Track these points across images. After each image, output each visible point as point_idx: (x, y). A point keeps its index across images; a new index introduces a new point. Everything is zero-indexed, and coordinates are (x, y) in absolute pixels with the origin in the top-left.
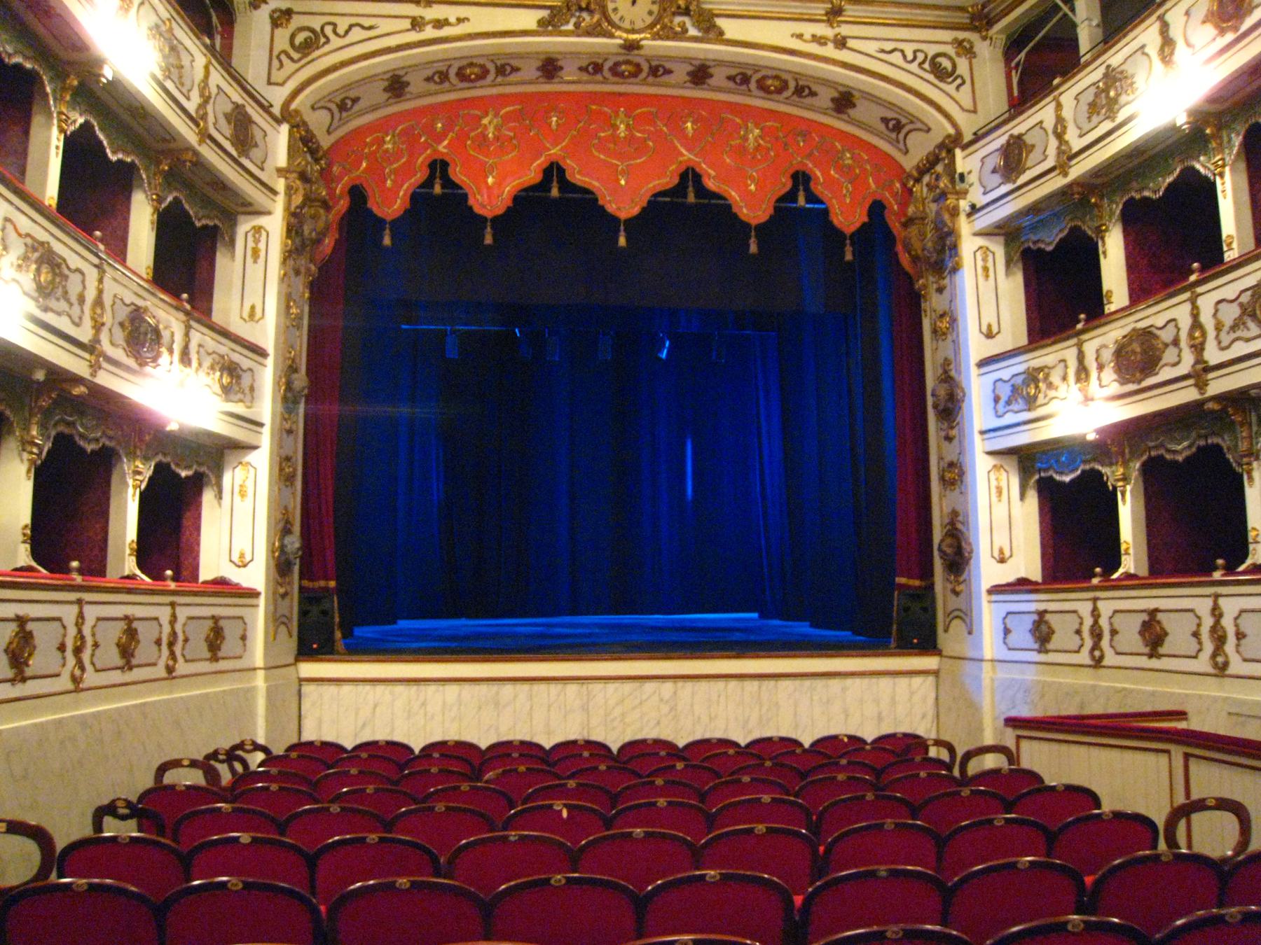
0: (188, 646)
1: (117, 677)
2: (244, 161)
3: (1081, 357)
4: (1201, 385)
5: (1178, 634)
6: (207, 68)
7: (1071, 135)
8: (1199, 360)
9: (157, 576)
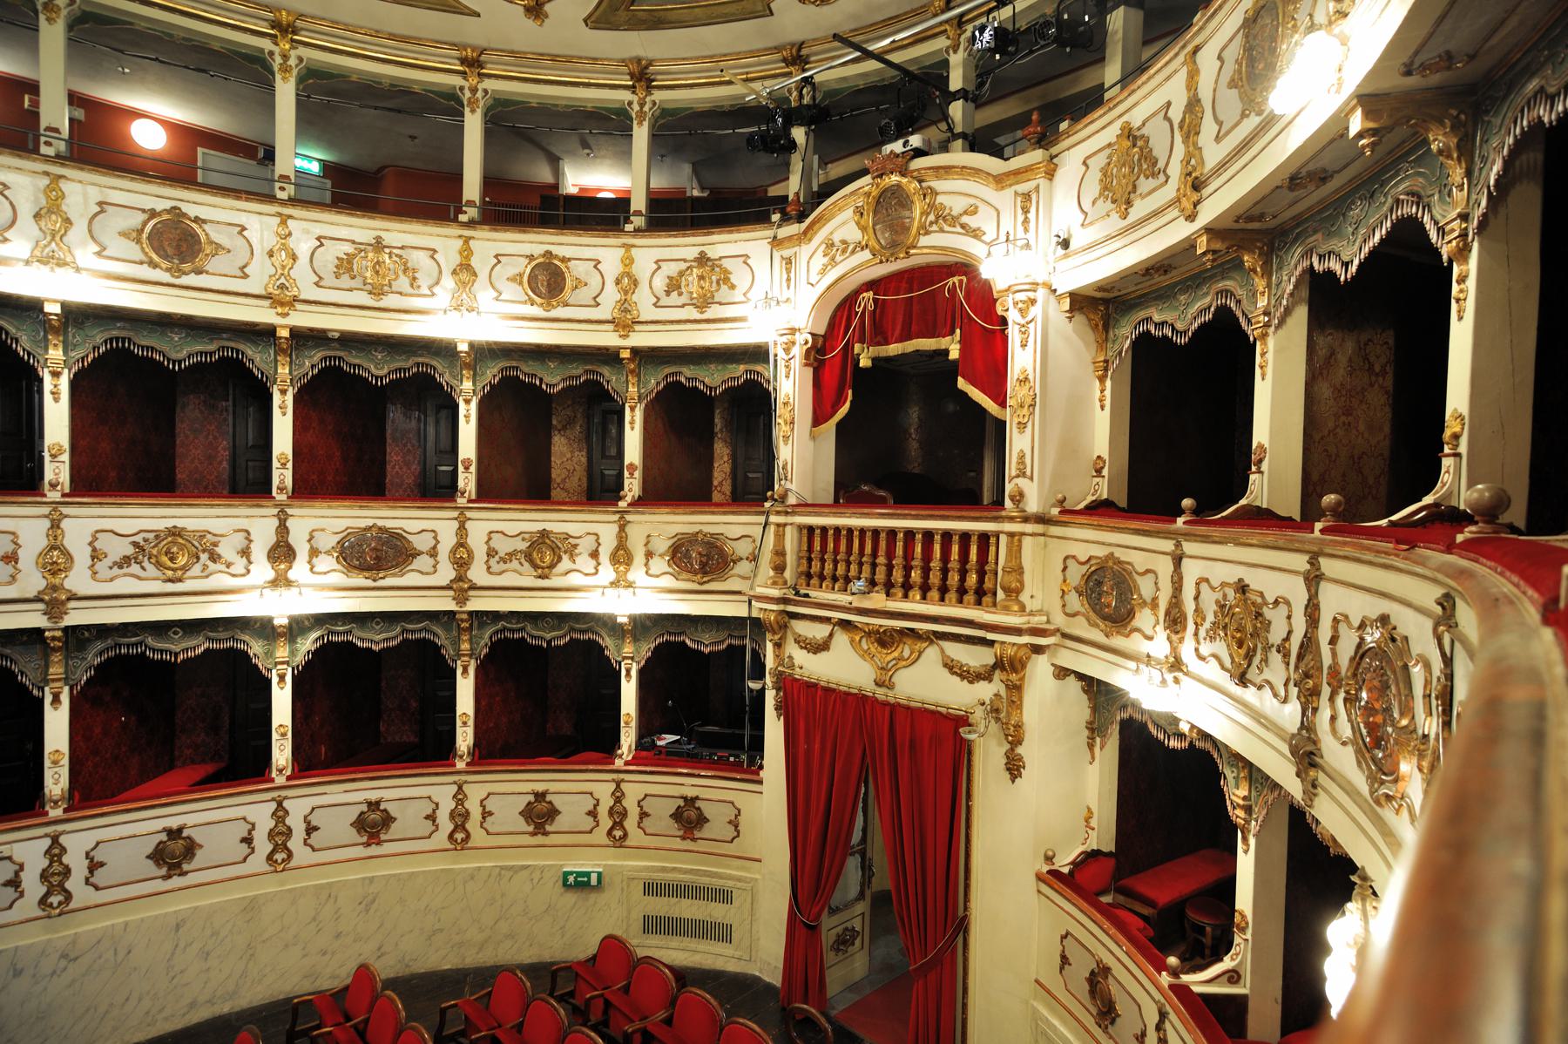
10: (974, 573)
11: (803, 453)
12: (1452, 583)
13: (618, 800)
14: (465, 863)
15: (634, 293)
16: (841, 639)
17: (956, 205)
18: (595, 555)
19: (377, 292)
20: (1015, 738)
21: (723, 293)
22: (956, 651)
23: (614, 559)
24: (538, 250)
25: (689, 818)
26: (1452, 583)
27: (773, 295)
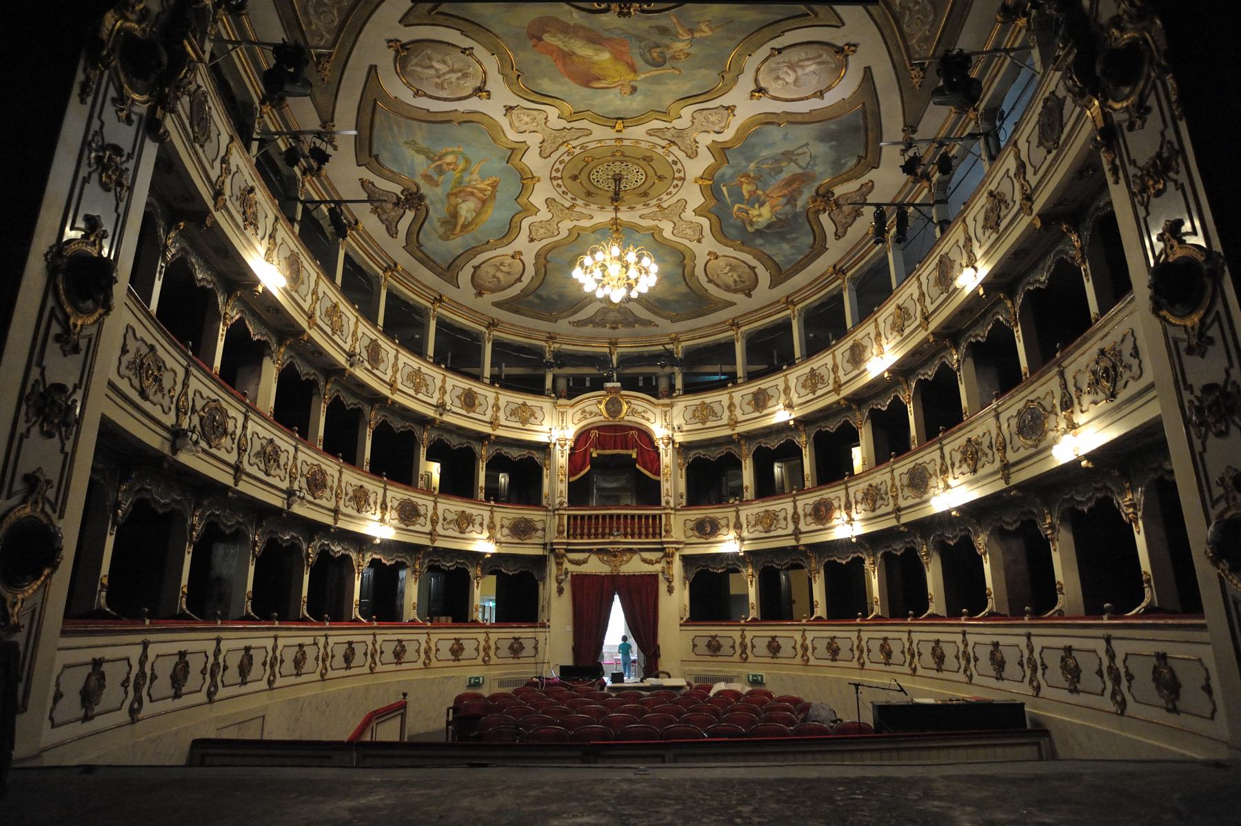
0: (156, 683)
1: (393, 667)
2: (375, 371)
4: (797, 540)
6: (356, 323)
8: (796, 528)
10: (653, 527)
11: (556, 484)
12: (403, 677)
13: (487, 642)
15: (495, 412)
16: (594, 559)
17: (640, 409)
18: (481, 525)
20: (669, 581)
21: (532, 419)
22: (646, 555)
24: (467, 387)
25: (516, 649)
26: (403, 677)
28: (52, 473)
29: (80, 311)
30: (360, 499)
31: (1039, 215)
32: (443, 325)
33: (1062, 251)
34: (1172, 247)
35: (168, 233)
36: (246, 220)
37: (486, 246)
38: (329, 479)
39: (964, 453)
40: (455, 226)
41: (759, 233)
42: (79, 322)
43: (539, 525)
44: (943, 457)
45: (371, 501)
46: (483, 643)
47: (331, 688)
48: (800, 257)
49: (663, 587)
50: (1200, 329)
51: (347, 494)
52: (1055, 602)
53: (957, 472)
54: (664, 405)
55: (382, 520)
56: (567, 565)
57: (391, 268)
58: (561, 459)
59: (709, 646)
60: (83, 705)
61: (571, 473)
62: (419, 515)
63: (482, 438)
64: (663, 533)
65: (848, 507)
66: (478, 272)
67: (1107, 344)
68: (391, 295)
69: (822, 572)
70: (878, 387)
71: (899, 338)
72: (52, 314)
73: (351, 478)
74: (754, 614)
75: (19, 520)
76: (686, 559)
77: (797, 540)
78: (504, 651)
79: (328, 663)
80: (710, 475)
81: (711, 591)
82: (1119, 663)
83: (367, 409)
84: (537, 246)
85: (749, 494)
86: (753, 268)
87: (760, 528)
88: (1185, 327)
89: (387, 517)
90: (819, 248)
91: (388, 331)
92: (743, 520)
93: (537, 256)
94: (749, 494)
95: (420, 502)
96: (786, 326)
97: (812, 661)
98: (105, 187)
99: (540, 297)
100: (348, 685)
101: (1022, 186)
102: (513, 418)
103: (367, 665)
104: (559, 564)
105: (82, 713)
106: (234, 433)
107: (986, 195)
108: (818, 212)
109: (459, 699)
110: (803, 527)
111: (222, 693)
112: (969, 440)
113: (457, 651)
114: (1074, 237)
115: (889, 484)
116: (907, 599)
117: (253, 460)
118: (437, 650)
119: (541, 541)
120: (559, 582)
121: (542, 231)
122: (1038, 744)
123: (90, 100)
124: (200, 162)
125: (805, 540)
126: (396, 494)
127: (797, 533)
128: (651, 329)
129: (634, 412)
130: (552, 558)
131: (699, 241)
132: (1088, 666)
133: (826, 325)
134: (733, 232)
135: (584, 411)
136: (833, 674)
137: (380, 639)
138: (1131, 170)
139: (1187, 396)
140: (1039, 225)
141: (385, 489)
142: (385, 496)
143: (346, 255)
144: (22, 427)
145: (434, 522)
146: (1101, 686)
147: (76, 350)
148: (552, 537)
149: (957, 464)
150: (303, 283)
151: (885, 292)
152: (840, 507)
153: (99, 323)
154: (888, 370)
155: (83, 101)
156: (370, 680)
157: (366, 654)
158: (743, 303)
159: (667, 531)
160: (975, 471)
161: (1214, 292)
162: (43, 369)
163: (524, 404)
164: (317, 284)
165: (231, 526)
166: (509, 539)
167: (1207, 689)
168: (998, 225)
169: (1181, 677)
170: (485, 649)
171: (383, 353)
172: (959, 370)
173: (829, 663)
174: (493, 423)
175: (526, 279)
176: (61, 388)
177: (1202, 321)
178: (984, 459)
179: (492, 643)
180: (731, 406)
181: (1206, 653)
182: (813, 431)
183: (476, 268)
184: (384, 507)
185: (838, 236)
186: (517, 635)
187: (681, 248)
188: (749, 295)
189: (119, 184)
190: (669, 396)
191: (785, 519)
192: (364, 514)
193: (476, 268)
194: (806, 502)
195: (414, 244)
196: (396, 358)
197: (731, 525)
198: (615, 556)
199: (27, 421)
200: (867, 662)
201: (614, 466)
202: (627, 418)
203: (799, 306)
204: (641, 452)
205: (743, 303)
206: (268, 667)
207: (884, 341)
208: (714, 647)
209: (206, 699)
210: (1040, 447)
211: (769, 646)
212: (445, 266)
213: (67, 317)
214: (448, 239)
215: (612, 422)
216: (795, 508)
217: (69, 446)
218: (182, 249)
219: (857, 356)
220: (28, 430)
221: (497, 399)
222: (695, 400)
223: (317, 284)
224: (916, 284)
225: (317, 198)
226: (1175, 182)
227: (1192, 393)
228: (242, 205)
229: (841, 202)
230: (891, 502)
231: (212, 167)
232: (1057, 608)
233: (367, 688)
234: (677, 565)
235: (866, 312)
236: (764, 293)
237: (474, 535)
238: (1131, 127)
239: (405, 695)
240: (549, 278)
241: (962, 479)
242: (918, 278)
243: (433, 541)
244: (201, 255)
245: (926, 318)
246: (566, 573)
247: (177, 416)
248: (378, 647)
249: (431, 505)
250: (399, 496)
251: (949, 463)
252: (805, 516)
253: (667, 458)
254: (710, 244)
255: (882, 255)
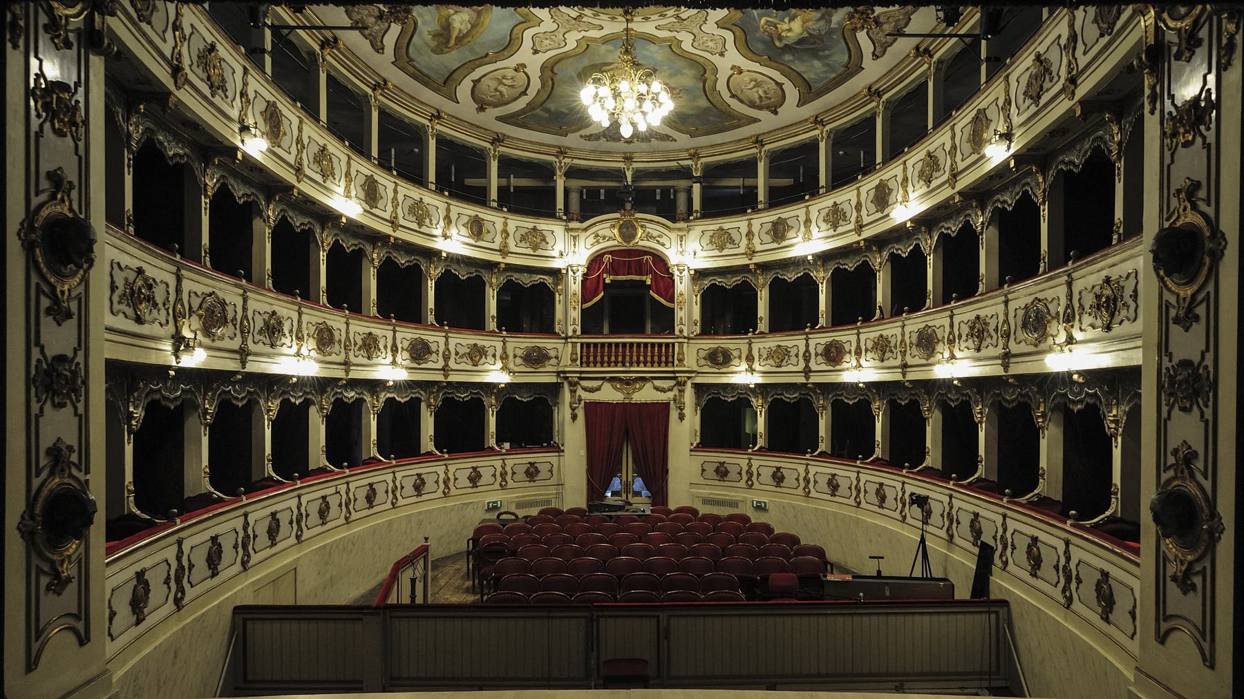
1: (415, 499)
3: (807, 213)
4: (807, 378)
5: (790, 479)
6: (349, 163)
7: (756, 240)
8: (807, 366)
9: (442, 325)
10: (666, 355)
11: (568, 311)
13: (503, 468)
14: (450, 503)
16: (607, 386)
17: (655, 234)
18: (494, 356)
19: (535, 249)
22: (657, 383)
23: (502, 358)
24: (473, 213)
25: (532, 473)
27: (571, 251)
28: (71, 439)
29: (62, 276)
30: (370, 345)
31: (1080, 102)
32: (442, 141)
33: (1101, 138)
34: (1185, 210)
35: (128, 119)
36: (211, 87)
37: (483, 60)
38: (336, 333)
39: (972, 328)
40: (448, 40)
41: (788, 48)
42: (66, 287)
43: (552, 353)
44: (952, 326)
45: (381, 346)
46: (499, 470)
47: (356, 529)
48: (833, 75)
49: (674, 414)
50: (1191, 303)
51: (355, 344)
52: (1036, 485)
53: (963, 345)
54: (680, 229)
55: (394, 363)
56: (580, 392)
57: (381, 85)
58: (575, 286)
59: (717, 471)
60: (134, 612)
61: (584, 300)
62: (430, 353)
63: (491, 266)
64: (676, 362)
65: (858, 353)
66: (479, 85)
67: (1114, 273)
68: (383, 114)
69: (829, 408)
70: (899, 234)
71: (924, 189)
72: (39, 290)
73: (359, 328)
74: (761, 442)
75: (51, 491)
76: (698, 388)
77: (807, 378)
78: (521, 475)
79: (351, 507)
80: (727, 306)
81: (723, 420)
82: (1073, 565)
83: (368, 248)
84: (542, 58)
85: (763, 326)
86: (780, 85)
87: (771, 362)
88: (1178, 295)
89: (399, 359)
90: (853, 68)
91: (384, 164)
92: (755, 353)
93: (543, 68)
94: (763, 326)
95: (431, 339)
96: (812, 146)
97: (813, 494)
98: (59, 133)
99: (548, 111)
100: (372, 523)
101: (1070, 63)
102: (523, 244)
103: (343, 515)
104: (573, 392)
105: (134, 619)
106: (234, 319)
107: (1032, 57)
108: (855, 30)
109: (479, 531)
110: (813, 366)
111: (255, 558)
112: (978, 317)
113: (475, 478)
114: (1115, 129)
115: (899, 338)
116: (905, 452)
117: (258, 337)
118: (456, 479)
119: (554, 369)
120: (573, 409)
121: (547, 42)
122: (997, 613)
123: (21, 43)
124: (151, 42)
125: (814, 379)
126: (407, 334)
127: (807, 371)
128: (669, 145)
129: (649, 237)
130: (566, 385)
131: (722, 54)
132: (1048, 558)
133: (853, 156)
134: (760, 46)
135: (597, 236)
136: (831, 508)
137: (399, 476)
138: (1168, 106)
139: (1165, 359)
140: (1078, 113)
141: (395, 332)
142: (394, 338)
143: (329, 76)
144: (35, 408)
145: (446, 358)
146: (1056, 579)
147: (69, 315)
148: (566, 363)
149: (964, 337)
150: (285, 134)
151: (918, 135)
152: (850, 352)
153: (85, 281)
154: (911, 220)
155: (15, 46)
156: (393, 515)
157: (387, 492)
158: (767, 121)
159: (679, 360)
160: (978, 350)
161: (1210, 270)
162: (42, 348)
163: (535, 229)
164: (300, 130)
165: (243, 399)
166: (523, 369)
167: (1133, 614)
168: (1039, 97)
169: (1117, 597)
170: (501, 475)
171: (381, 188)
172: (982, 233)
173: (828, 497)
174: (504, 251)
175: (532, 93)
176: (61, 359)
177: (1194, 296)
178: (989, 340)
179: (508, 469)
180: (750, 234)
181: (1136, 585)
182: (832, 266)
183: (476, 82)
184: (395, 350)
185: (875, 56)
186: (532, 460)
187: (701, 61)
188: (776, 113)
189: (73, 123)
190: (686, 220)
191: (797, 355)
192: (375, 361)
193: (476, 82)
194: (819, 341)
195: (403, 58)
196: (395, 191)
197: (744, 357)
198: (628, 384)
199: (38, 401)
200: (863, 501)
201: (628, 301)
202: (641, 243)
203: (828, 127)
204: (656, 278)
205: (767, 121)
206: (295, 525)
207: (910, 188)
208: (722, 472)
209: (241, 569)
210: (1039, 348)
211: (774, 476)
212: (441, 81)
213: (53, 288)
214: (442, 52)
215: (626, 246)
216: (807, 346)
217: (81, 406)
218: (146, 130)
219: (882, 198)
220: (41, 409)
221: (506, 224)
222: (713, 225)
223: (300, 130)
224: (949, 134)
225: (292, 23)
226: (1204, 138)
227: (1170, 361)
228: (205, 70)
229: (881, 20)
230: (900, 357)
231: (165, 41)
232: (1036, 492)
233: (390, 523)
234: (689, 394)
235: (894, 152)
236: (791, 111)
237: (487, 367)
238: (1178, 57)
239: (426, 539)
240: (557, 91)
241: (967, 353)
242: (952, 129)
243: (446, 376)
244: (167, 129)
245: (955, 176)
246: (580, 400)
247: (176, 321)
248: (398, 484)
249: (442, 341)
250: (409, 336)
251: (957, 333)
252: (817, 355)
253: (682, 286)
254: (734, 57)
255: (923, 80)
